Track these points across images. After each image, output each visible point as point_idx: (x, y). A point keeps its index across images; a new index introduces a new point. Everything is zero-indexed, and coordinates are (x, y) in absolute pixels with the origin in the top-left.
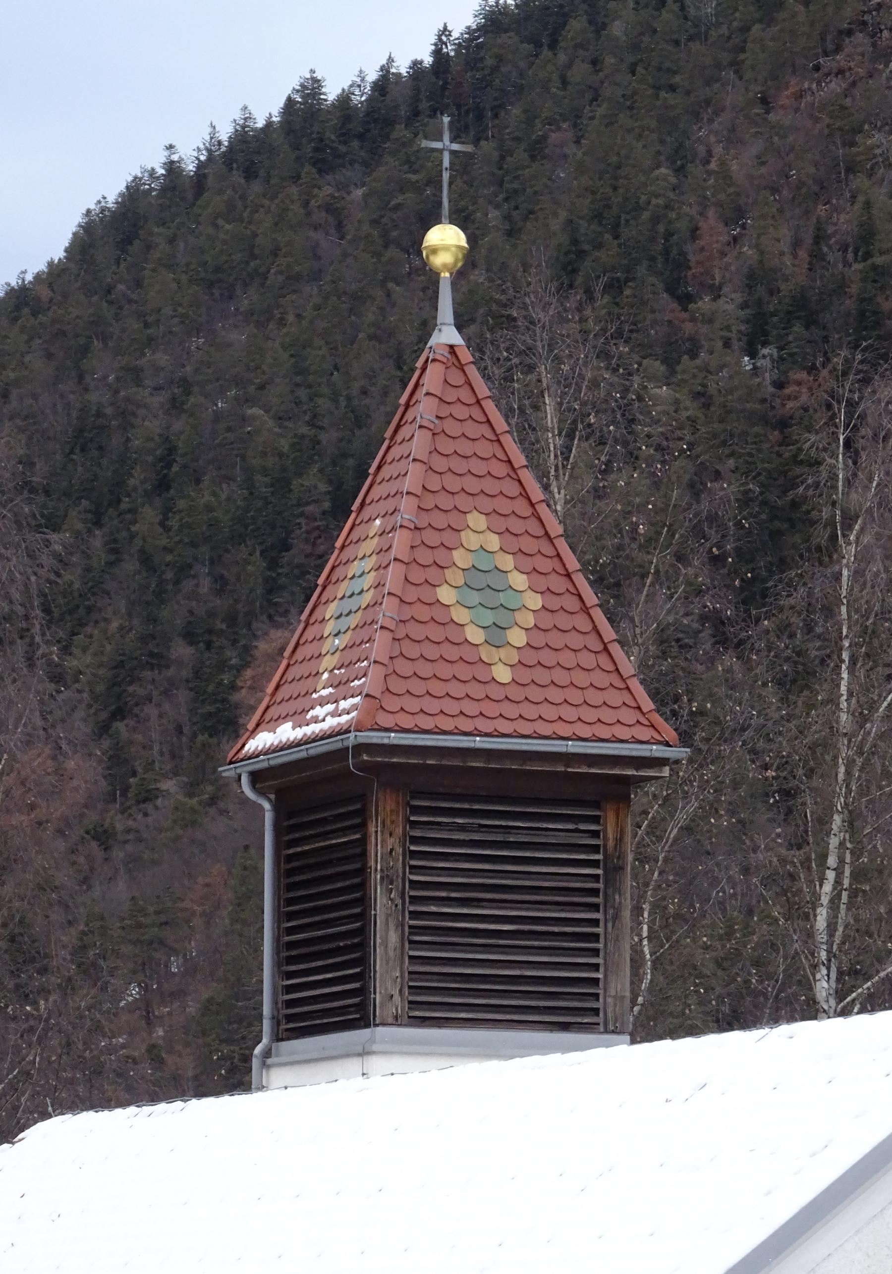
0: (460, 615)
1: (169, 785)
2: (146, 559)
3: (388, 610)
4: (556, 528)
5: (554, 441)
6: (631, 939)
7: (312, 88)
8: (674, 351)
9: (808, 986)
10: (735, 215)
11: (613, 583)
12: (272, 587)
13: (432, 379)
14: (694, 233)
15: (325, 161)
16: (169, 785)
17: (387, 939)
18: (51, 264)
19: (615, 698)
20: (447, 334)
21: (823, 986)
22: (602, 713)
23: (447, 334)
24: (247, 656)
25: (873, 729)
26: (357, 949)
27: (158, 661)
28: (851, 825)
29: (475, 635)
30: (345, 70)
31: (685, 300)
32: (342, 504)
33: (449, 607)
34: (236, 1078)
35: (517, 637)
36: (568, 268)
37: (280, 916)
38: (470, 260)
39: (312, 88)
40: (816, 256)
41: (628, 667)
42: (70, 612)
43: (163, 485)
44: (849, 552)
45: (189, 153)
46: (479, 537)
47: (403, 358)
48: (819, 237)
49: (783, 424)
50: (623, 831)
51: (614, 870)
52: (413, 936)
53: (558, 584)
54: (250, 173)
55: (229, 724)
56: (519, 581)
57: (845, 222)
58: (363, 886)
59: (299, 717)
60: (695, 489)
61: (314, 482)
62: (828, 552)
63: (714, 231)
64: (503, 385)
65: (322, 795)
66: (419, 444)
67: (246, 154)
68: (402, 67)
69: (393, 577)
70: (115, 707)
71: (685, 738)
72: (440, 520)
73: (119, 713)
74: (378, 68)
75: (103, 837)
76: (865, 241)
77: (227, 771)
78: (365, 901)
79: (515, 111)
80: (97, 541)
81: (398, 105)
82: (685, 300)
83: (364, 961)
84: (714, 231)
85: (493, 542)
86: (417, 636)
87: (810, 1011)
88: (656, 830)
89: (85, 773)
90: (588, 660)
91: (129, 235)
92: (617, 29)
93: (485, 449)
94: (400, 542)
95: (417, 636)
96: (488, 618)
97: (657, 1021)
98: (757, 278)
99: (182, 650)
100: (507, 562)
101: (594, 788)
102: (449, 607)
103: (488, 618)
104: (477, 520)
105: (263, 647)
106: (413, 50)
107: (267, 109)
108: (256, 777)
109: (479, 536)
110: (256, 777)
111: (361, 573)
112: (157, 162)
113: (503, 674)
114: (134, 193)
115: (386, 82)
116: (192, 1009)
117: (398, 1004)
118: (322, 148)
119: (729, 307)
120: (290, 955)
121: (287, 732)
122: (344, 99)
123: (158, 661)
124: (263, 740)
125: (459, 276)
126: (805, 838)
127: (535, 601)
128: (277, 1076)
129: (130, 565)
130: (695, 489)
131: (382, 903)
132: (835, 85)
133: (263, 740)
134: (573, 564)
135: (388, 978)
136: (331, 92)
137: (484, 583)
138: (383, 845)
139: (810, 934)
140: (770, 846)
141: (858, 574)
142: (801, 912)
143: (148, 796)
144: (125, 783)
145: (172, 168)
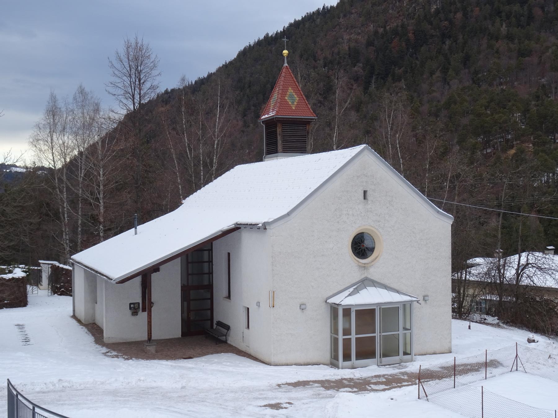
0: (288, 101)
1: (251, 125)
2: (248, 96)
3: (279, 100)
4: (300, 89)
5: (300, 78)
6: (311, 142)
7: (267, 34)
8: (315, 68)
9: (333, 148)
10: (322, 50)
11: (308, 97)
12: (264, 100)
13: (284, 70)
14: (317, 53)
15: (269, 44)
16: (251, 125)
17: (280, 142)
18: (295, 21)
19: (308, 111)
20: (286, 64)
21: (335, 147)
22: (307, 114)
23: (286, 64)
24: (261, 108)
25: (341, 115)
26: (276, 143)
27: (250, 109)
28: (338, 127)
29: (290, 103)
30: (272, 32)
31: (316, 61)
32: (272, 88)
33: (287, 99)
34: (261, 160)
35: (296, 103)
36: (301, 56)
37: (266, 140)
38: (289, 54)
39: (267, 34)
40: (333, 55)
41: (310, 107)
42: (239, 102)
43: (250, 86)
44: (337, 92)
45: (252, 43)
46: (290, 91)
47: (280, 69)
48: (333, 53)
49: (328, 77)
50: (310, 128)
51: (308, 133)
52: (283, 142)
53: (301, 96)
54: (260, 46)
55: (259, 116)
56: (296, 96)
57: (336, 51)
58: (276, 135)
59: (268, 114)
60: (318, 85)
61: (269, 86)
62: (334, 93)
63: (319, 52)
64: (293, 72)
65: (271, 124)
66: (282, 79)
67: (259, 43)
68: (279, 32)
69: (280, 96)
70: (244, 115)
71: (317, 116)
72: (285, 88)
73: (245, 116)
74: (234, 222)
75: (243, 131)
76: (339, 53)
77: (259, 121)
78: (277, 137)
79: (294, 37)
80: (242, 93)
81: (279, 36)
82: (316, 61)
83: (277, 145)
84: (319, 52)
85: (292, 91)
86: (283, 104)
87: (333, 150)
88: (314, 128)
89: (241, 123)
90: (304, 106)
91: (244, 54)
92: (307, 26)
93: (291, 79)
94: (280, 91)
95: (283, 104)
96: (292, 101)
97: (314, 152)
98: (325, 58)
99: (253, 108)
100: (294, 94)
101: (305, 123)
102: (287, 99)
103: (292, 101)
104: (290, 88)
105: (263, 107)
106: (280, 29)
107: (262, 37)
108: (263, 122)
109: (290, 91)
110: (263, 122)
111: (275, 96)
112: (248, 45)
113: (294, 108)
114: (245, 49)
115: (277, 33)
116: (255, 153)
117: (281, 150)
118: (270, 43)
119: (321, 62)
120: (267, 144)
121: (266, 116)
122: (272, 36)
123: (250, 109)
124: (264, 117)
125: (288, 57)
126: (332, 129)
127: (298, 99)
128: (266, 160)
129: (246, 97)
130: (318, 85)
131: (279, 138)
132: (335, 33)
133: (264, 117)
134: (302, 94)
135: (280, 147)
136: (270, 35)
137: (291, 96)
138: (279, 130)
139: (333, 141)
140: (327, 130)
141: (338, 95)
142: (332, 139)
143: (249, 126)
144: (246, 125)
145: (250, 45)
